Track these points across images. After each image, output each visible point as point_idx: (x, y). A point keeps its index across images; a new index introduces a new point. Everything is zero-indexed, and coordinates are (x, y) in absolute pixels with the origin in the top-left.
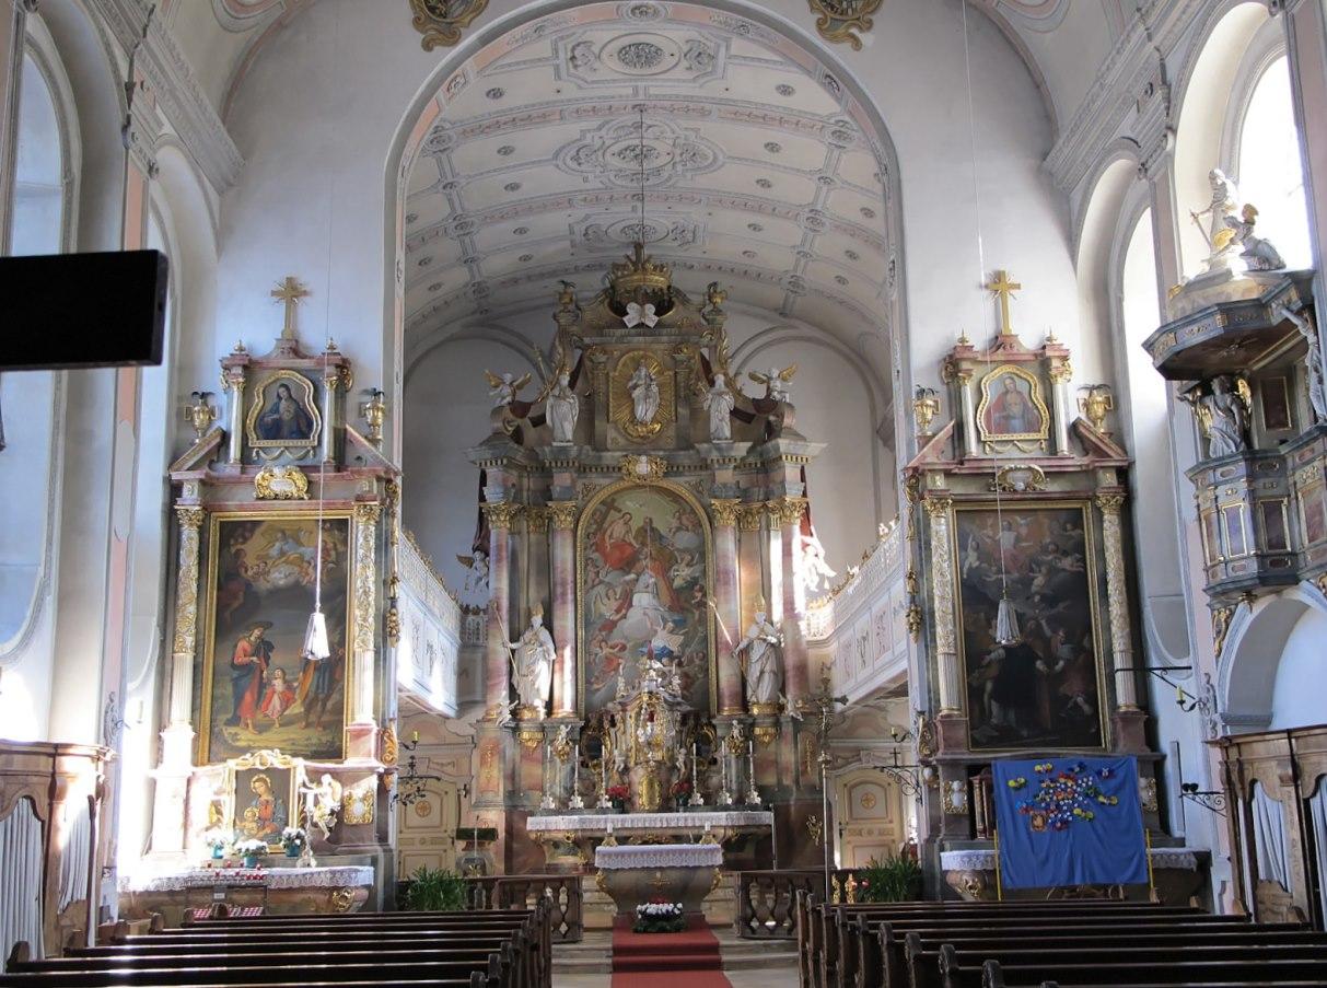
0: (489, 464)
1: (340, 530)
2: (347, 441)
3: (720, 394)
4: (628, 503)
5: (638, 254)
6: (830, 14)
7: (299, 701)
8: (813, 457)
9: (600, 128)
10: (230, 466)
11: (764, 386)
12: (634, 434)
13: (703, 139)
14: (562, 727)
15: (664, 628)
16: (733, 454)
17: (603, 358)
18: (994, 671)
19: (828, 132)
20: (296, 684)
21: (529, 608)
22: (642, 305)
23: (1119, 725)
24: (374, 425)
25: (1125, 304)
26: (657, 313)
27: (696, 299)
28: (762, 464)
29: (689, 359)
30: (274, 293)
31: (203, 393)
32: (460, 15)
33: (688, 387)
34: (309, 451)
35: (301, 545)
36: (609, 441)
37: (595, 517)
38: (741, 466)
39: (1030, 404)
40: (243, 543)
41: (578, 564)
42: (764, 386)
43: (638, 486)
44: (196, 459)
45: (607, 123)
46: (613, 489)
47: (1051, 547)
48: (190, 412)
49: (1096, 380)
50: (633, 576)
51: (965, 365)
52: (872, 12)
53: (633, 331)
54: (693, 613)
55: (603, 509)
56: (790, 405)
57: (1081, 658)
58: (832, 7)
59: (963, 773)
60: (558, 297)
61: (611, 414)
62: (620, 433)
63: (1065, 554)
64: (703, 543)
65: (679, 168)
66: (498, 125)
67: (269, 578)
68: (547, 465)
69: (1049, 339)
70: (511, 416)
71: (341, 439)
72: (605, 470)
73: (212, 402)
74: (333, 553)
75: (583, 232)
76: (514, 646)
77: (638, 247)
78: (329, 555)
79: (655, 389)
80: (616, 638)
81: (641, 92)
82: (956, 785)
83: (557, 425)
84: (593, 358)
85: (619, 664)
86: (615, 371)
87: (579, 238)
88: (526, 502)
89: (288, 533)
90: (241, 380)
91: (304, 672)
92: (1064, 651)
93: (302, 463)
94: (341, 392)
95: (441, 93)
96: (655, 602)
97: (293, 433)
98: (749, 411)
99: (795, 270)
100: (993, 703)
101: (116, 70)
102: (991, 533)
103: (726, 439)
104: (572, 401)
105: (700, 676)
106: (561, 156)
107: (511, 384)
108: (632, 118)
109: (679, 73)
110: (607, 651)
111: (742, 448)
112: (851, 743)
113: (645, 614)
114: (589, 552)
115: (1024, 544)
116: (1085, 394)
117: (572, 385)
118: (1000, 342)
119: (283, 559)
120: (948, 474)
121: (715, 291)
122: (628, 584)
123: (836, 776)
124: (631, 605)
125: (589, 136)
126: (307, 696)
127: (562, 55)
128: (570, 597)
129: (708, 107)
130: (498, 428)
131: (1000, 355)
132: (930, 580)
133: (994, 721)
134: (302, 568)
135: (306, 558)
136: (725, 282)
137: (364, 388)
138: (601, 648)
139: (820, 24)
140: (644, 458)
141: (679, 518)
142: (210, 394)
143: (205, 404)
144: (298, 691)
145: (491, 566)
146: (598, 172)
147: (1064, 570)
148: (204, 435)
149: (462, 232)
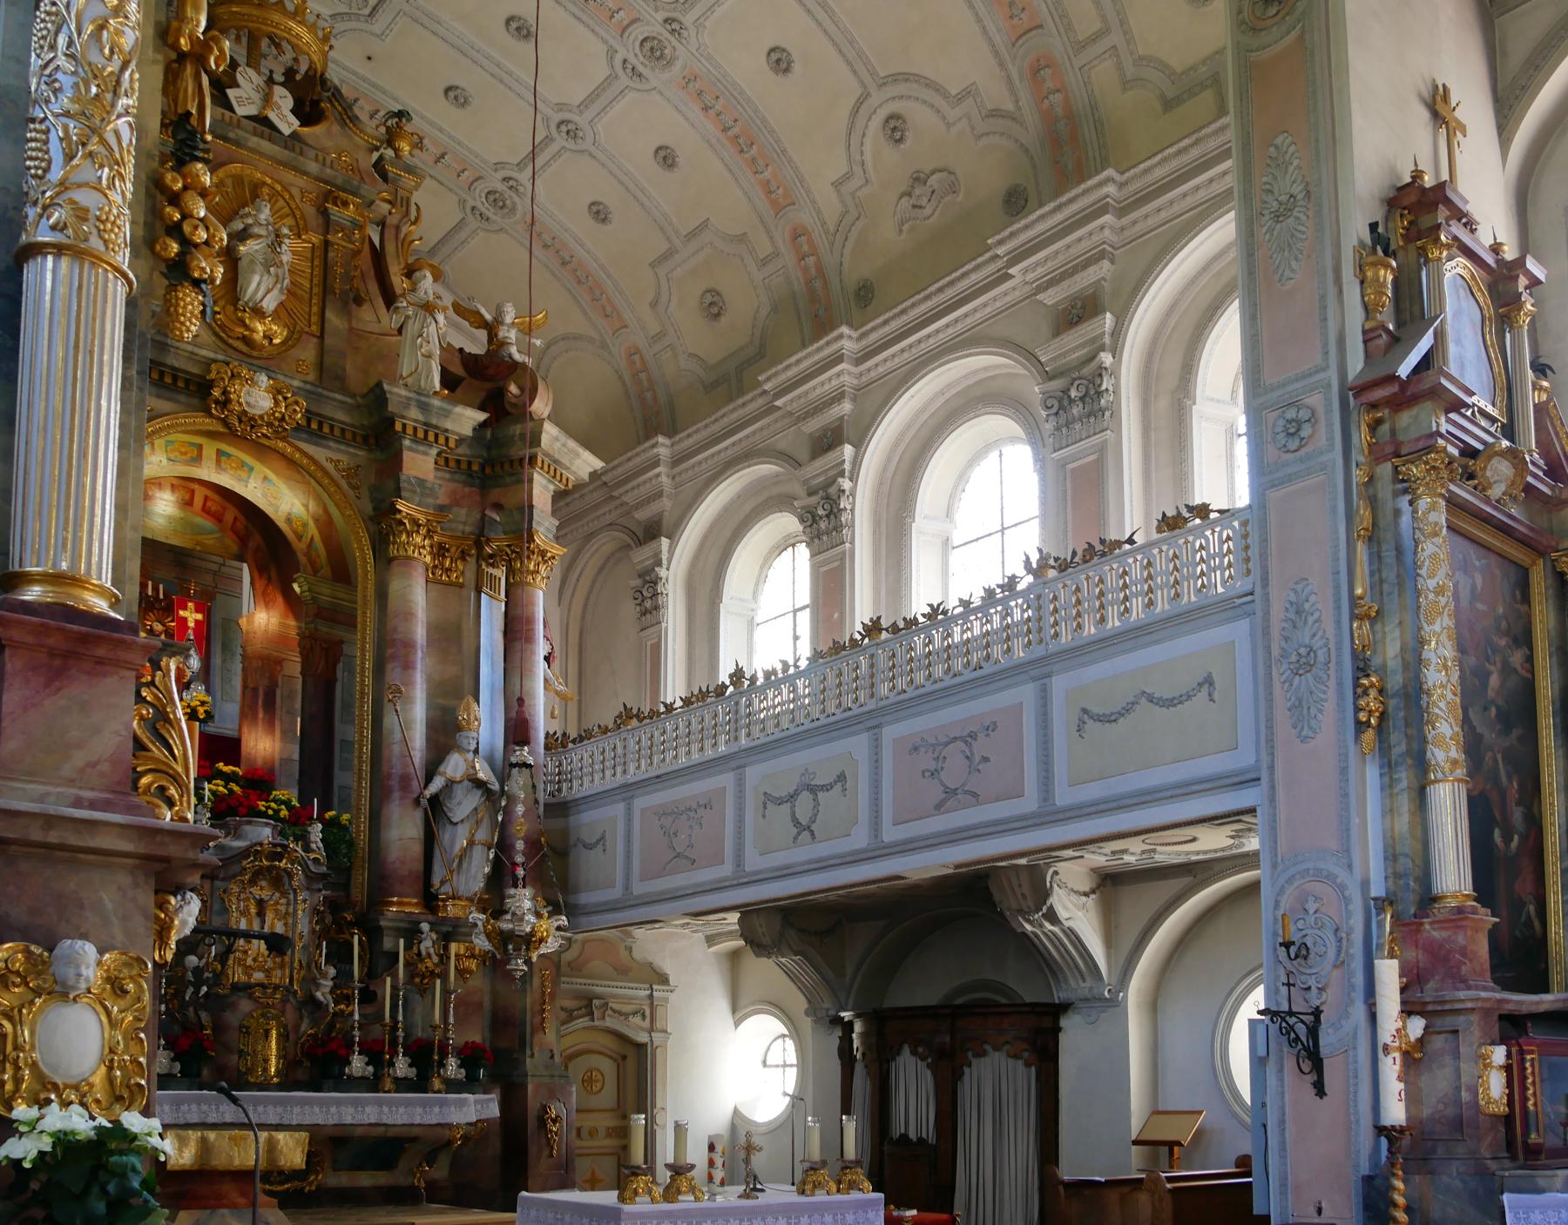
16: (448, 425)
140: (263, 379)
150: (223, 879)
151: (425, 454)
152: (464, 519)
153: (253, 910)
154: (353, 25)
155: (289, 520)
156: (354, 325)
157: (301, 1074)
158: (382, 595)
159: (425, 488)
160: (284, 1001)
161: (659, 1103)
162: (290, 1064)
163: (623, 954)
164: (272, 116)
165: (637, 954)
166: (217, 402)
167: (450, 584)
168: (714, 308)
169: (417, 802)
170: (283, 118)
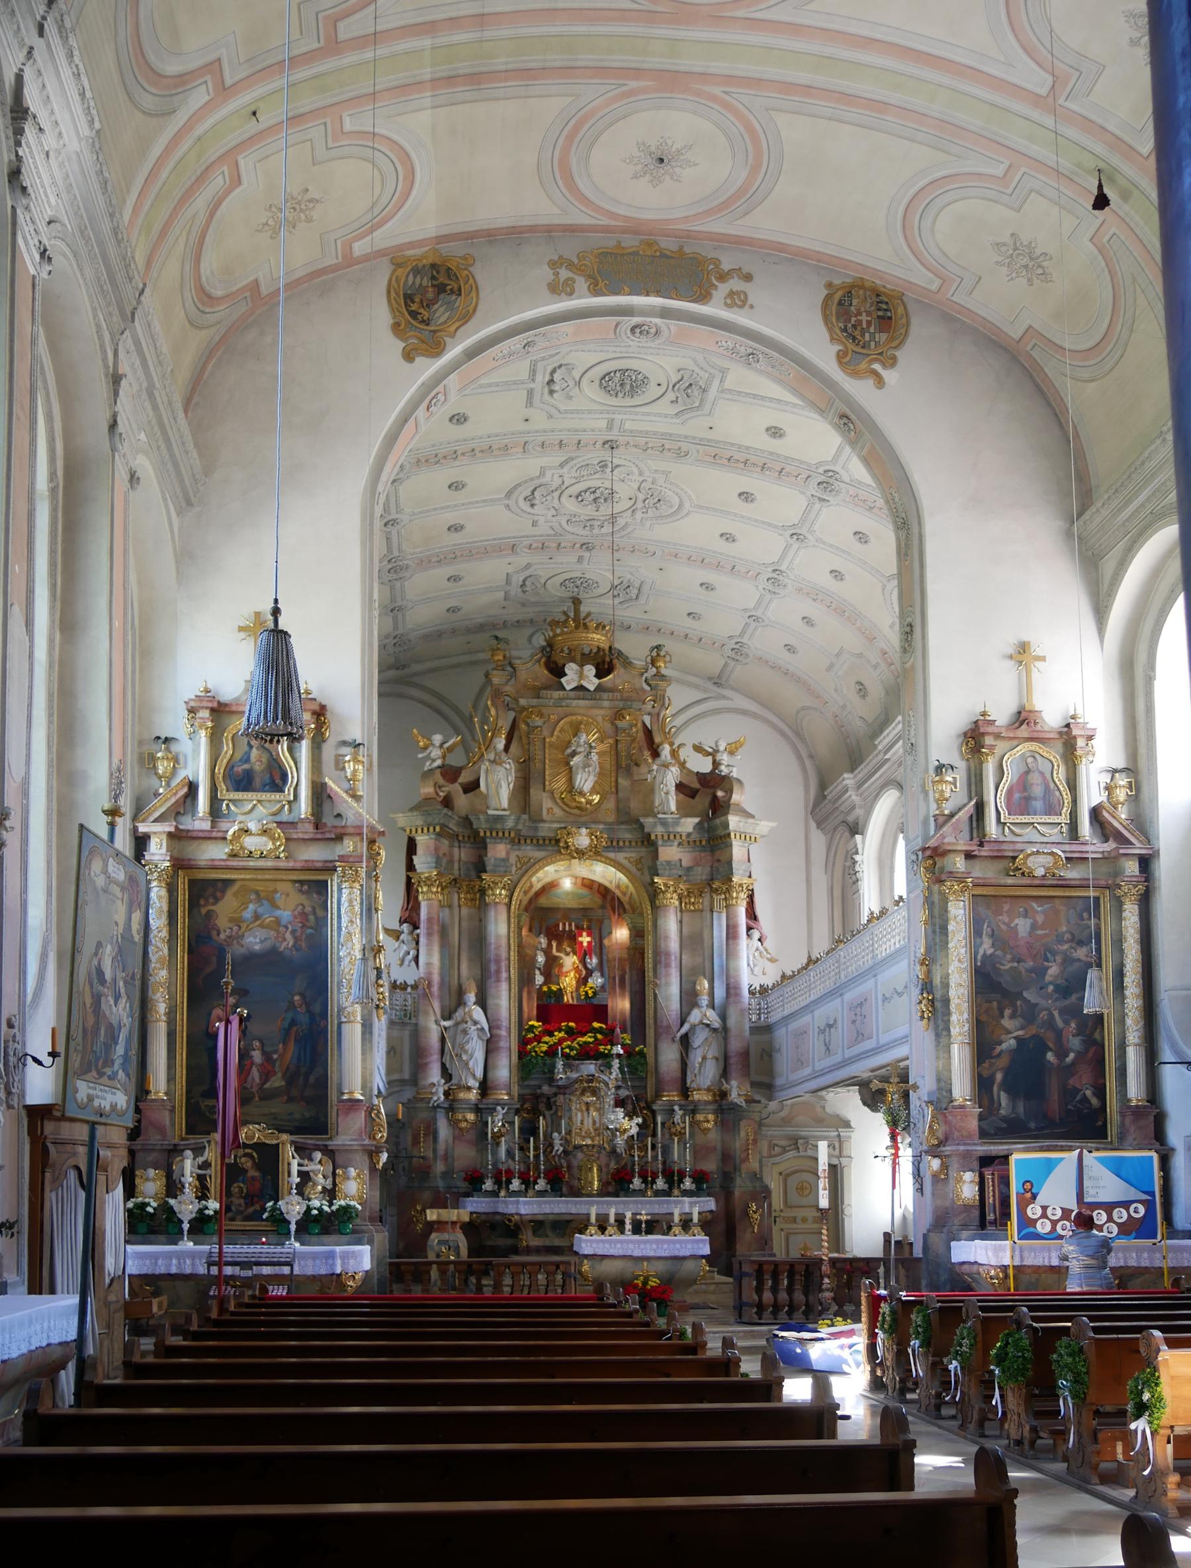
1: (319, 893)
2: (325, 796)
3: (666, 766)
6: (851, 346)
7: (279, 1075)
8: (763, 836)
9: (562, 465)
10: (200, 820)
13: (671, 483)
14: (499, 1108)
16: (679, 829)
17: (538, 722)
18: (1004, 1062)
19: (813, 482)
20: (275, 1056)
21: (460, 986)
22: (582, 666)
23: (1128, 1120)
24: (354, 778)
25: (1156, 683)
26: (599, 675)
27: (639, 663)
28: (708, 841)
30: (241, 629)
31: (166, 739)
32: (445, 322)
33: (629, 756)
35: (278, 908)
38: (688, 842)
39: (1052, 785)
40: (215, 904)
44: (162, 810)
45: (572, 459)
47: (1067, 936)
48: (152, 759)
49: (1120, 763)
51: (988, 740)
52: (896, 348)
53: (572, 694)
56: (739, 781)
57: (1092, 1050)
58: (854, 338)
59: (976, 1165)
62: (557, 803)
63: (1081, 943)
65: (639, 515)
66: (455, 455)
67: (243, 942)
68: (482, 834)
69: (1073, 717)
70: (441, 781)
71: (320, 794)
72: (541, 842)
73: (175, 748)
74: (312, 918)
76: (447, 1024)
77: (577, 602)
78: (307, 920)
79: (594, 757)
81: (616, 424)
82: (968, 1176)
83: (492, 791)
87: (515, 590)
88: (456, 872)
89: (262, 894)
90: (210, 724)
92: (1075, 1043)
93: (278, 819)
94: (318, 742)
95: (421, 412)
97: (265, 785)
99: (742, 635)
100: (1002, 1093)
101: (105, 359)
102: (1007, 920)
104: (508, 766)
106: (514, 496)
107: (441, 746)
108: (597, 455)
109: (664, 406)
111: (689, 824)
112: (789, 1130)
115: (1040, 932)
116: (1106, 778)
117: (507, 749)
118: (1023, 718)
119: (258, 923)
120: (969, 856)
121: (658, 655)
125: (549, 474)
126: (288, 1068)
127: (539, 378)
129: (685, 447)
131: (1023, 732)
132: (945, 966)
133: (1003, 1112)
134: (278, 932)
135: (284, 922)
136: (670, 646)
137: (341, 739)
139: (840, 357)
140: (584, 831)
142: (173, 739)
143: (168, 750)
144: (277, 1064)
145: (422, 940)
146: (549, 517)
147: (1079, 960)
148: (168, 784)
149: (395, 576)
152: (701, 873)
153: (584, 1108)
155: (618, 887)
156: (636, 778)
157: (611, 1189)
158: (655, 925)
160: (599, 1153)
161: (846, 1202)
162: (604, 1184)
163: (819, 1110)
165: (827, 1110)
168: (862, 690)
169: (673, 1041)
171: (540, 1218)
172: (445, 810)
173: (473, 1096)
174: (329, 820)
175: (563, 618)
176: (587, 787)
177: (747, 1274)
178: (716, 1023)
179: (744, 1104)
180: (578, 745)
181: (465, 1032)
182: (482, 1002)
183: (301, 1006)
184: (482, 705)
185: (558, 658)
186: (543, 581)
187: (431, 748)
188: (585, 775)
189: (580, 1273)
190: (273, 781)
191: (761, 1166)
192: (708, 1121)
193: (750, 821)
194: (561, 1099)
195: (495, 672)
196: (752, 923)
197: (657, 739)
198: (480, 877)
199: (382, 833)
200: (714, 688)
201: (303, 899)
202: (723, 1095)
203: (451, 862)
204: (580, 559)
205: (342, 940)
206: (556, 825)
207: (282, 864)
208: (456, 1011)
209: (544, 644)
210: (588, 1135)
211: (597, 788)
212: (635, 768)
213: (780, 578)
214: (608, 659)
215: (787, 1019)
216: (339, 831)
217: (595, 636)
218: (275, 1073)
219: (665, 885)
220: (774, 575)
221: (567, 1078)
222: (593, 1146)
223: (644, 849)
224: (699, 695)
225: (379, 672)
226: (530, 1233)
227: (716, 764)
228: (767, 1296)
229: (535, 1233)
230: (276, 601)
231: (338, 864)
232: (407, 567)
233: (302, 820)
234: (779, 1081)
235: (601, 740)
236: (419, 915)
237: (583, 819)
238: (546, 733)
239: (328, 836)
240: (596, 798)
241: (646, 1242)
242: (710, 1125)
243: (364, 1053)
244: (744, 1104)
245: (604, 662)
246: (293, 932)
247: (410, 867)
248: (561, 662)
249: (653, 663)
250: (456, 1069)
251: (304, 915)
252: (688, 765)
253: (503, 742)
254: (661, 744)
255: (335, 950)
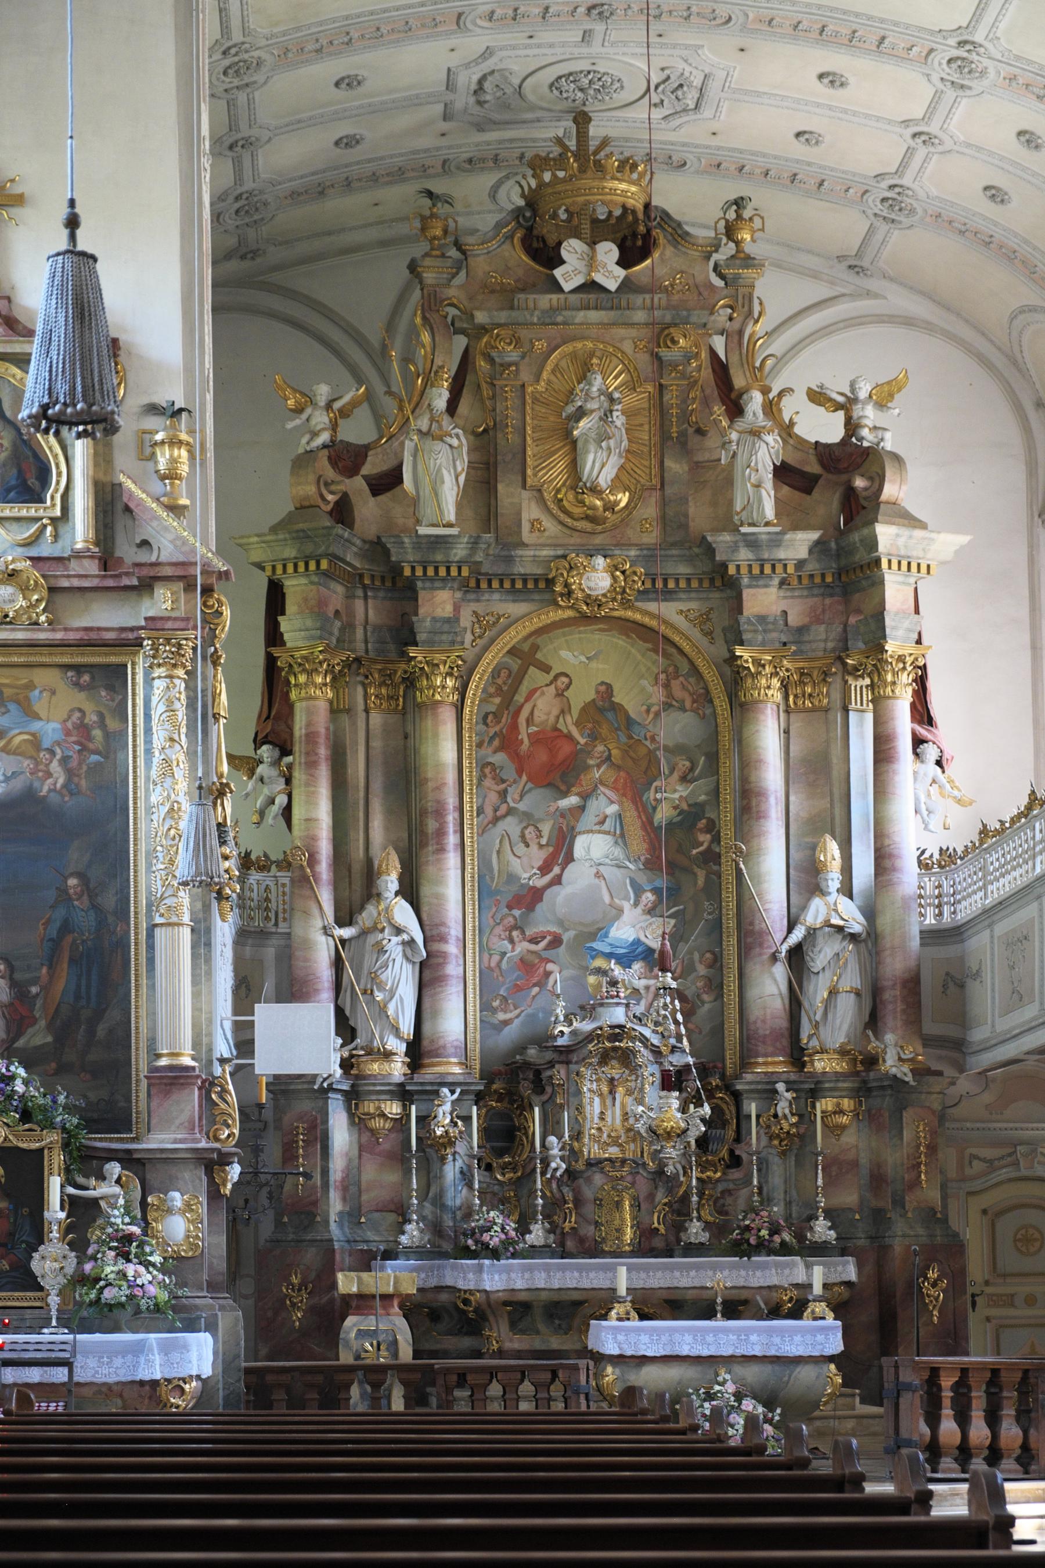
0: (290, 568)
1: (110, 688)
2: (119, 507)
3: (756, 433)
4: (564, 654)
5: (582, 135)
7: (43, 1023)
8: (943, 563)
11: (841, 414)
12: (577, 511)
14: (445, 1091)
15: (636, 904)
16: (782, 554)
21: (369, 862)
24: (171, 476)
26: (624, 262)
28: (838, 574)
29: (688, 358)
33: (685, 416)
34: (45, 526)
35: (37, 717)
36: (526, 527)
37: (500, 681)
41: (466, 772)
42: (841, 414)
43: (584, 619)
46: (537, 623)
50: (573, 800)
53: (573, 298)
54: (695, 874)
55: (515, 664)
56: (897, 458)
60: (417, 224)
61: (529, 472)
62: (548, 510)
64: (714, 735)
68: (407, 572)
70: (330, 473)
72: (519, 585)
74: (97, 733)
75: (474, 86)
76: (346, 933)
77: (582, 119)
78: (90, 738)
79: (619, 419)
80: (542, 922)
83: (426, 491)
84: (494, 354)
85: (547, 974)
86: (537, 381)
87: (463, 100)
88: (360, 646)
91: (50, 967)
93: (34, 552)
96: (618, 852)
97: (8, 490)
98: (808, 469)
99: (899, 172)
103: (767, 524)
104: (455, 442)
105: (705, 997)
107: (329, 406)
110: (522, 947)
113: (598, 875)
114: (486, 751)
117: (452, 408)
121: (739, 217)
122: (563, 816)
123: (970, 1194)
124: (570, 858)
128: (452, 839)
130: (307, 498)
134: (37, 762)
135: (46, 744)
137: (146, 400)
138: (512, 941)
140: (600, 562)
141: (667, 686)
144: (39, 1003)
149: (236, 82)
150: (576, 1063)
151: (766, 586)
152: (824, 638)
153: (605, 1089)
154: (685, 119)
156: (699, 457)
159: (767, 623)
160: (634, 1174)
164: (599, 278)
166: (562, 595)
167: (814, 710)
170: (609, 274)
171: (523, 1297)
172: (339, 529)
173: (397, 1069)
174: (127, 552)
175: (556, 150)
176: (605, 479)
177: (909, 1387)
178: (857, 924)
179: (909, 1078)
180: (588, 397)
181: (381, 950)
182: (410, 892)
183: (80, 897)
184: (403, 325)
185: (547, 230)
186: (516, 82)
187: (309, 411)
188: (602, 455)
189: (599, 1389)
190: (25, 481)
191: (944, 1198)
192: (841, 1112)
193: (918, 533)
194: (559, 1073)
195: (428, 262)
196: (922, 731)
197: (739, 381)
198: (403, 654)
199: (224, 576)
200: (850, 277)
201: (80, 699)
202: (872, 1061)
203: (348, 627)
204: (587, 36)
205: (154, 774)
206: (546, 552)
207: (42, 636)
208: (362, 908)
209: (521, 203)
210: (615, 1142)
211: (625, 478)
212: (698, 438)
213: (974, 57)
214: (642, 229)
215: (989, 914)
216: (145, 572)
217: (616, 184)
218: (34, 1021)
219: (757, 662)
220: (961, 53)
221: (574, 1033)
222: (624, 1161)
223: (717, 595)
224: (823, 291)
225: (214, 263)
226: (504, 1326)
227: (852, 427)
228: (949, 1427)
229: (513, 1325)
230: (72, 203)
231: (143, 634)
232: (259, 63)
233: (77, 555)
234: (978, 1035)
235: (631, 386)
236: (291, 729)
237: (598, 540)
238: (525, 376)
239: (126, 581)
240: (623, 499)
241: (726, 1331)
242: (844, 1120)
243: (195, 981)
244: (909, 1078)
245: (634, 235)
246: (64, 761)
247: (274, 637)
248: (551, 240)
249: (730, 231)
250: (363, 1019)
251: (83, 729)
252: (797, 430)
253: (446, 395)
254: (746, 390)
255: (141, 793)
